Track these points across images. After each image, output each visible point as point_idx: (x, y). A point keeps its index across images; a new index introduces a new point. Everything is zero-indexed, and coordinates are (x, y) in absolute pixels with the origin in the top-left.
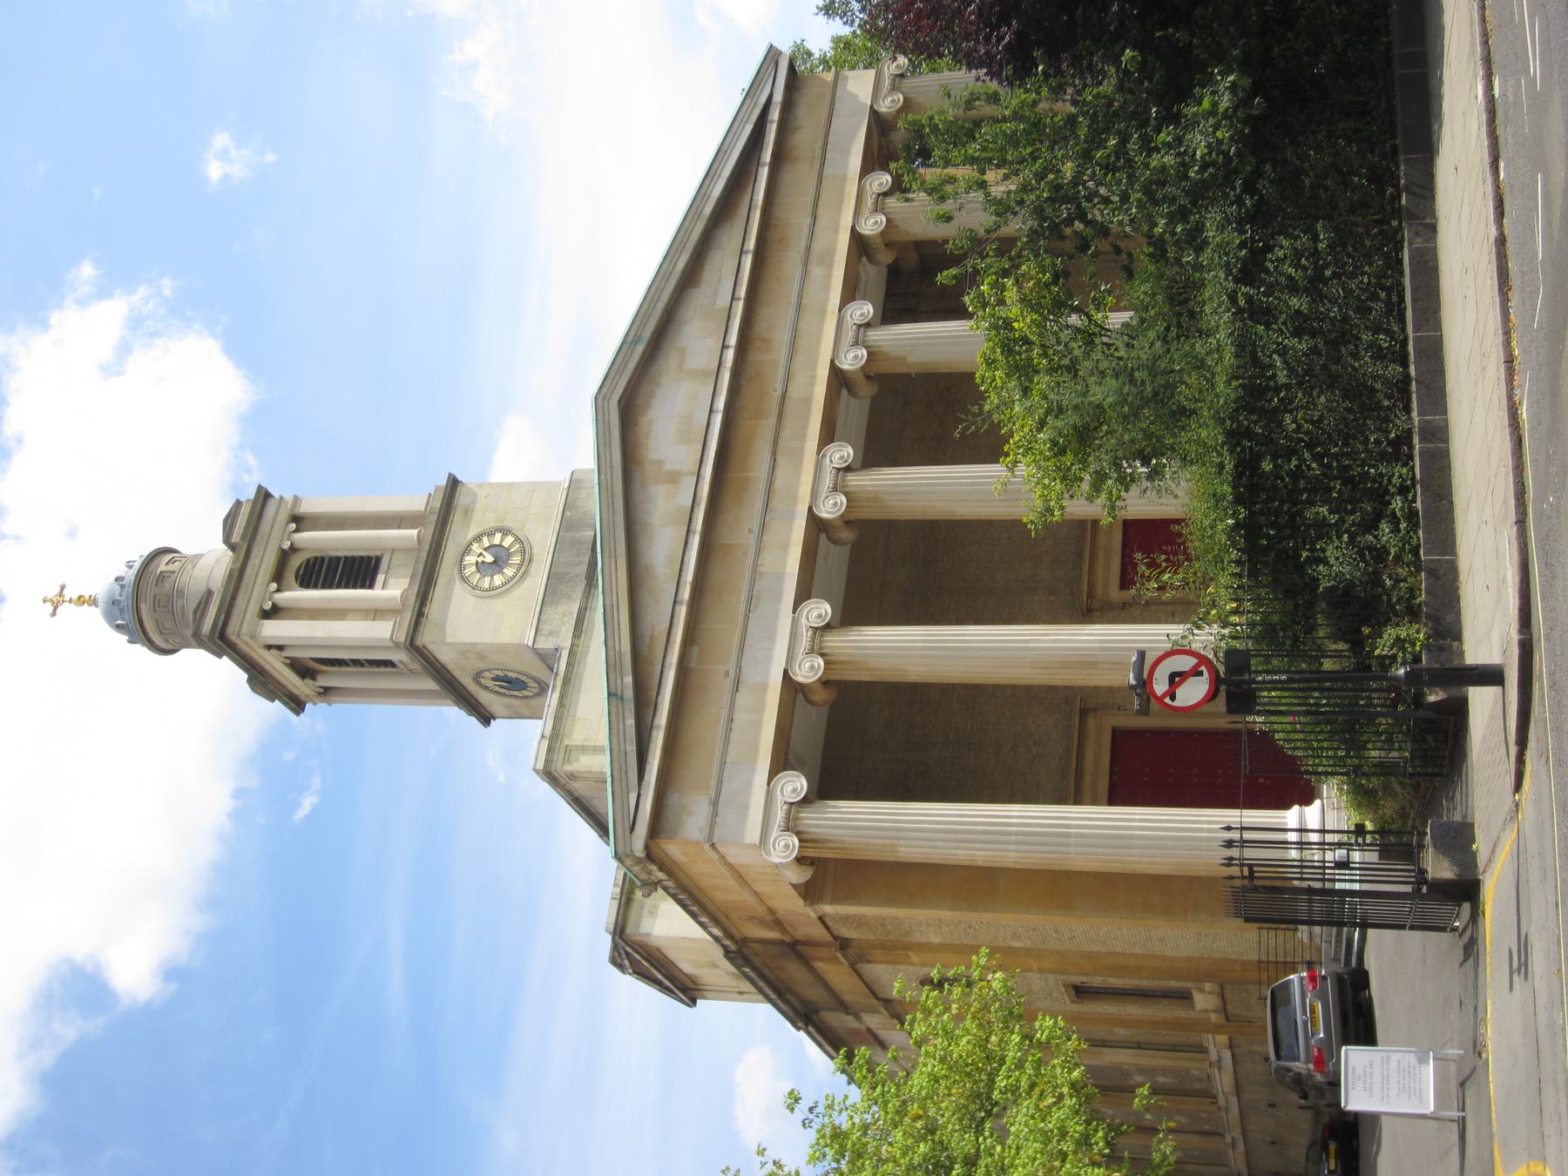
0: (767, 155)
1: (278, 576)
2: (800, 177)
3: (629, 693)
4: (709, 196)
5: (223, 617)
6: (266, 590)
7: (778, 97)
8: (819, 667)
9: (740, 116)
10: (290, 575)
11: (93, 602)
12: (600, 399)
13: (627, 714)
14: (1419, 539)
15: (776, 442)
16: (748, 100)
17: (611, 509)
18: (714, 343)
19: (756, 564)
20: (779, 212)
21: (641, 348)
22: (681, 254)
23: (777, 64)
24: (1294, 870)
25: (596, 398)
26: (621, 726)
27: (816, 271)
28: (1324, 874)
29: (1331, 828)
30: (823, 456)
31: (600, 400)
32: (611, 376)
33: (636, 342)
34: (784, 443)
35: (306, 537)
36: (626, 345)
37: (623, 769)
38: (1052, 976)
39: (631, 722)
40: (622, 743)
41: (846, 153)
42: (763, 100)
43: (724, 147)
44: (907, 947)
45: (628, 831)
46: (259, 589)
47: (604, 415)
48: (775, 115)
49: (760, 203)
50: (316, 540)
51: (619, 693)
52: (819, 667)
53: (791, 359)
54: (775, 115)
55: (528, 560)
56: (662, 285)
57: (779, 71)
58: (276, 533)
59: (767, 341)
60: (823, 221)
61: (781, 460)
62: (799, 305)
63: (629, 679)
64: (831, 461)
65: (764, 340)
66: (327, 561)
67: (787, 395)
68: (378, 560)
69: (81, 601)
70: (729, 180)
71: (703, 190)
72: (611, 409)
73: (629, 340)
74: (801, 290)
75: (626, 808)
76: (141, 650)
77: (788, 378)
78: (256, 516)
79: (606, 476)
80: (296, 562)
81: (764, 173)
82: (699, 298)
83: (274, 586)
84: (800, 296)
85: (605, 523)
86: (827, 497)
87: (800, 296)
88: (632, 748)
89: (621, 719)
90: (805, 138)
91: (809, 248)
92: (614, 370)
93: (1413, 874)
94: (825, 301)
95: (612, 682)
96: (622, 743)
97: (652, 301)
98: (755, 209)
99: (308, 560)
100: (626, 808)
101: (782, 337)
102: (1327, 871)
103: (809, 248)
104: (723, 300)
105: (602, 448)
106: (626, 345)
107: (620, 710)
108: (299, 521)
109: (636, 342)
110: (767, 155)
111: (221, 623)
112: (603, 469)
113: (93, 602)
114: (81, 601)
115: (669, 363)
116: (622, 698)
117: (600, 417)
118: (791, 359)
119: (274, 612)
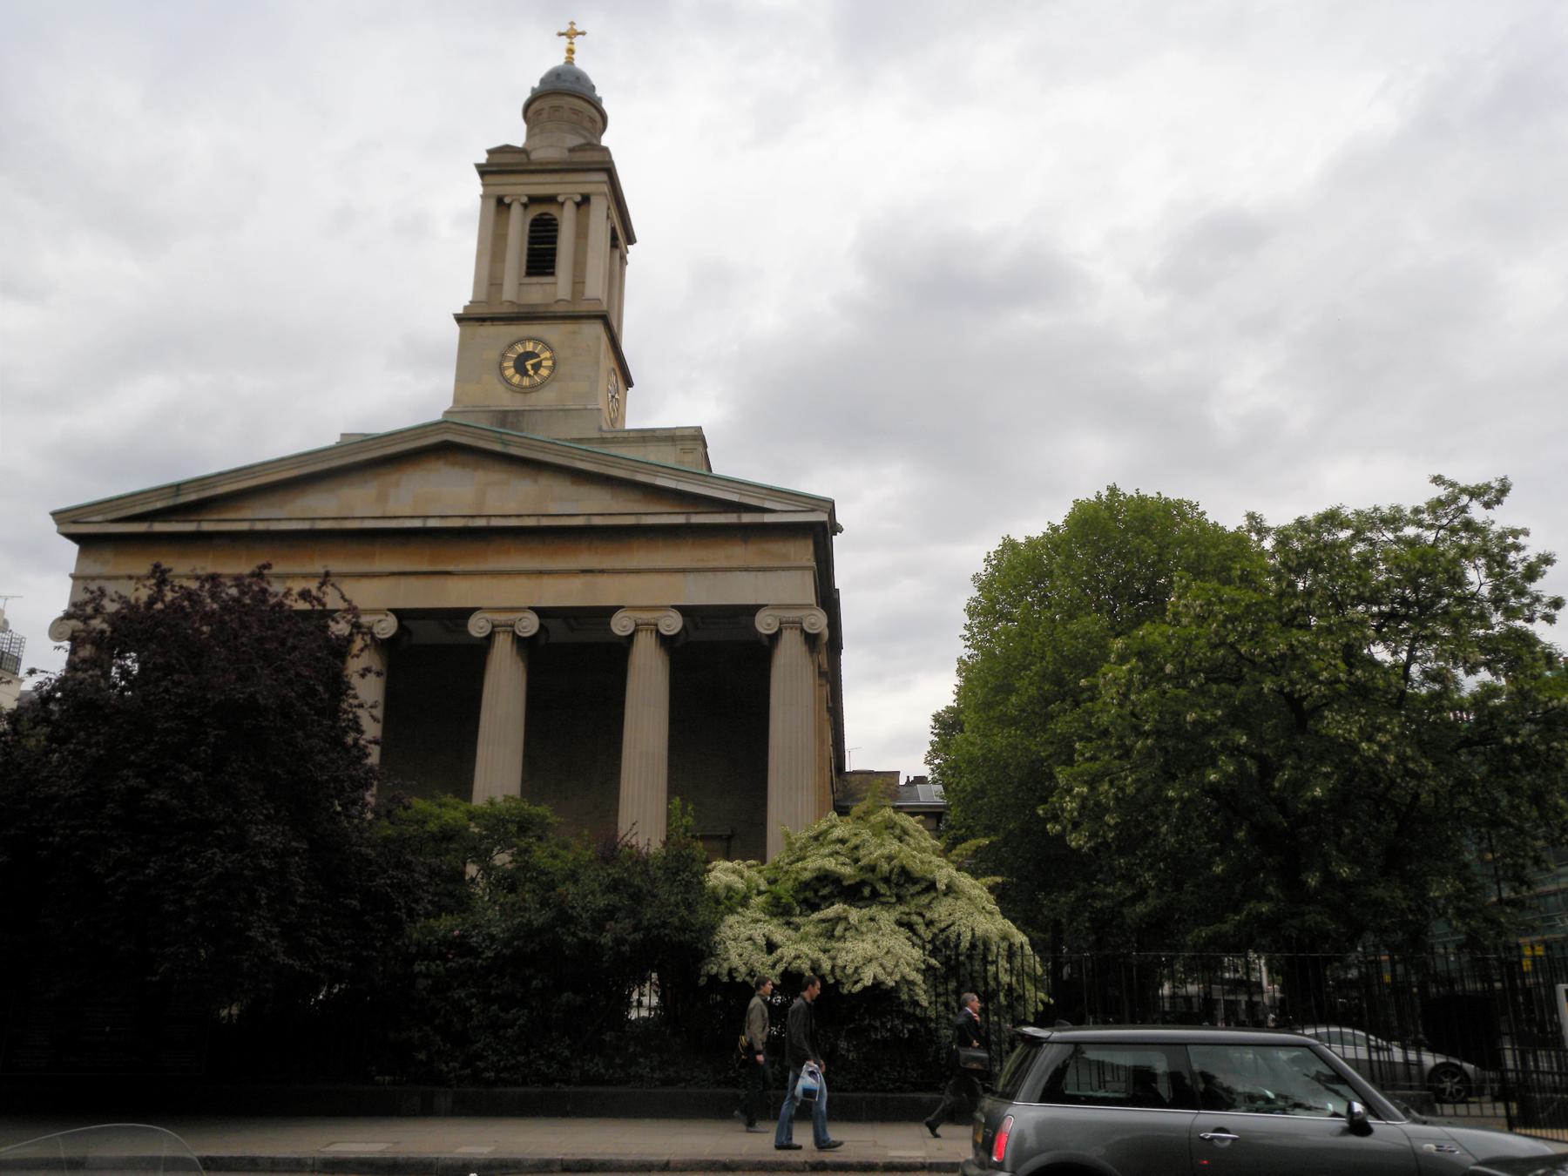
1: (534, 200)
3: (182, 500)
6: (520, 195)
7: (768, 518)
10: (536, 211)
11: (570, 61)
14: (891, 1091)
16: (764, 491)
23: (813, 510)
30: (387, 615)
39: (159, 505)
42: (767, 505)
44: (1320, 707)
45: (73, 519)
48: (747, 518)
50: (567, 220)
55: (525, 391)
57: (803, 514)
58: (570, 189)
63: (193, 497)
64: (380, 621)
66: (553, 234)
67: (449, 577)
69: (571, 51)
76: (527, 95)
78: (585, 167)
80: (552, 210)
83: (525, 200)
88: (138, 510)
90: (739, 553)
91: (602, 571)
93: (1553, 1053)
99: (555, 219)
103: (602, 571)
105: (399, 436)
113: (570, 61)
114: (571, 51)
117: (429, 429)
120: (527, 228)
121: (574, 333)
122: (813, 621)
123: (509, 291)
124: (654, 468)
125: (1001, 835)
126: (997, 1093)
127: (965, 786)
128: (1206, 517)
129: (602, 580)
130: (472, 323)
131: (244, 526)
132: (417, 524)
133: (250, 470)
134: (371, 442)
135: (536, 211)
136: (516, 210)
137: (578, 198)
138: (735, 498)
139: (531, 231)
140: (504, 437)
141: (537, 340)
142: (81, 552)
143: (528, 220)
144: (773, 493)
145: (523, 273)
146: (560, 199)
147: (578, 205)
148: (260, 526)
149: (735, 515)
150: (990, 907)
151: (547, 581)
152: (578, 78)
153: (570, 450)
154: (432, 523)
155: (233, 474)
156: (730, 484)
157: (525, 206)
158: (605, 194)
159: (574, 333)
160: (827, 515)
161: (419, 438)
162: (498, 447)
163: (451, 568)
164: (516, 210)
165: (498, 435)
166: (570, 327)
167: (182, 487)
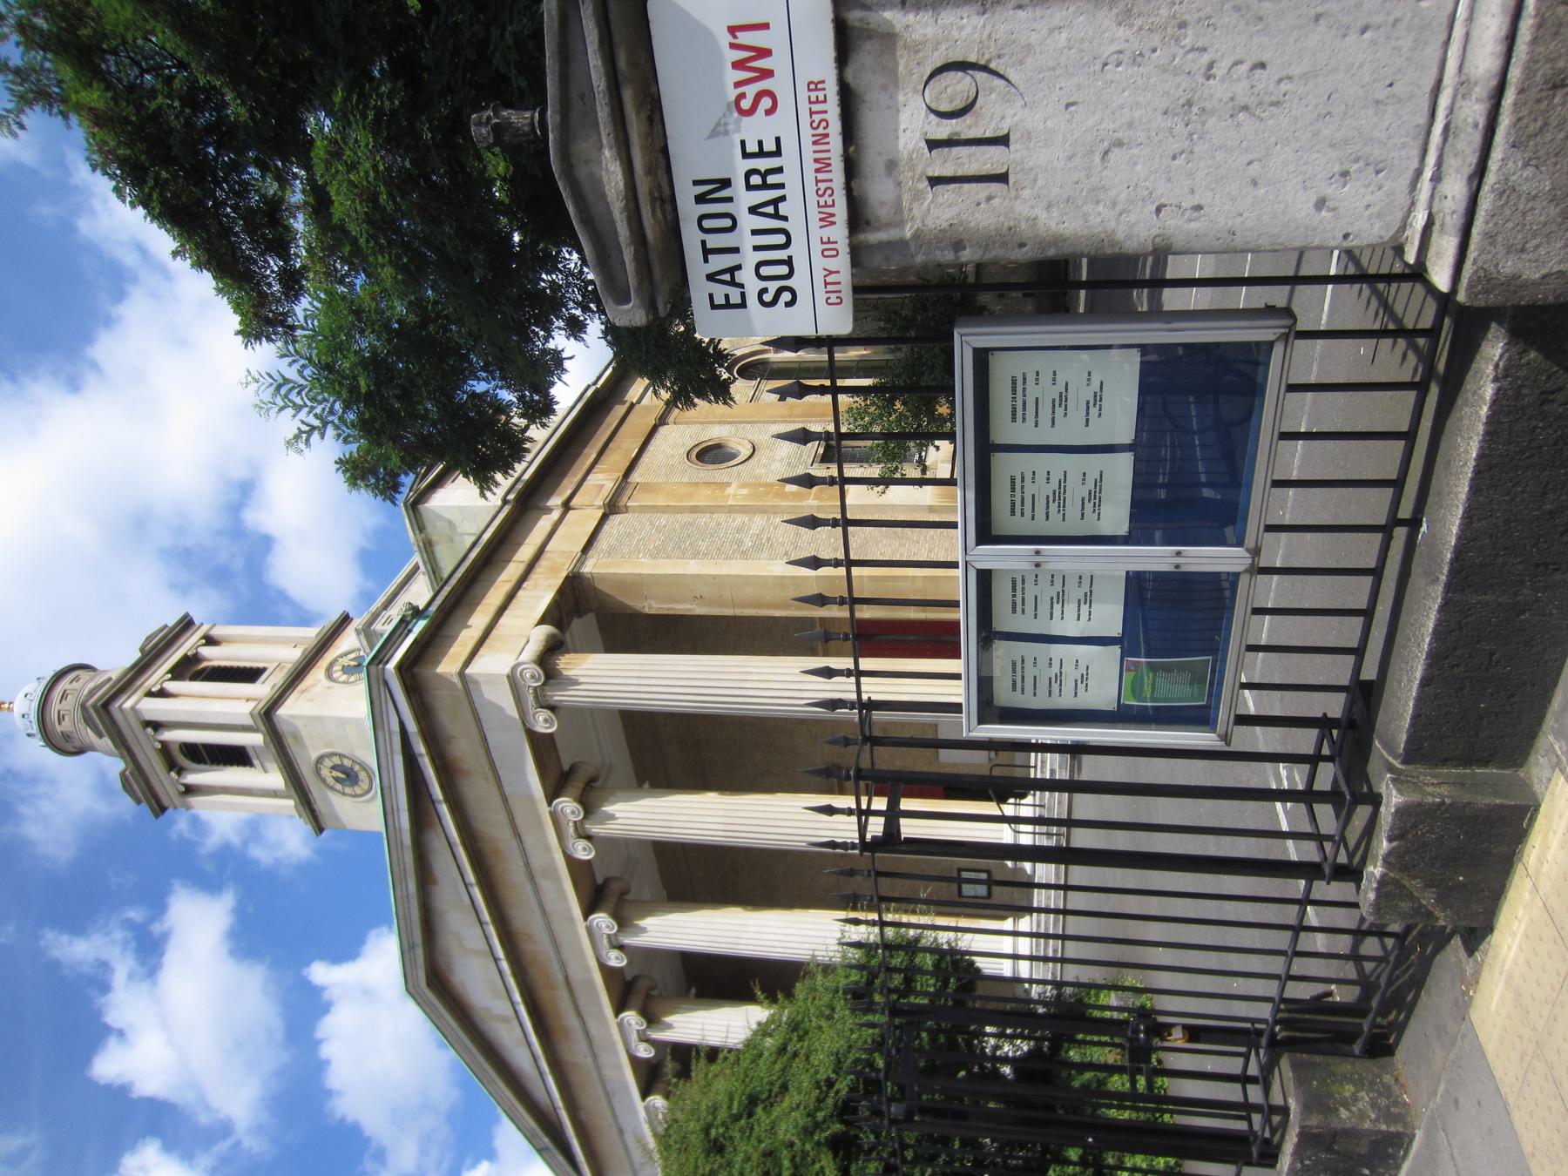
0: (437, 791)
2: (477, 791)
4: (400, 829)
5: (153, 802)
7: (412, 727)
8: (539, 674)
9: (382, 751)
12: (411, 989)
15: (577, 1008)
16: (380, 734)
19: (601, 1077)
21: (420, 951)
22: (406, 878)
23: (386, 684)
25: (407, 990)
27: (546, 885)
31: (411, 989)
32: (409, 972)
33: (412, 947)
34: (584, 1008)
35: (206, 651)
36: (406, 954)
38: (893, 929)
39: (561, 1158)
41: (522, 771)
42: (396, 727)
46: (158, 676)
47: (421, 997)
48: (420, 748)
50: (215, 656)
52: (539, 674)
54: (420, 748)
56: (406, 906)
60: (528, 839)
61: (588, 1019)
62: (544, 913)
65: (526, 935)
68: (264, 670)
70: (410, 810)
73: (406, 948)
77: (563, 966)
81: (444, 809)
85: (472, 1066)
90: (463, 748)
91: (527, 865)
92: (408, 965)
94: (569, 910)
97: (405, 920)
98: (456, 846)
105: (436, 1021)
106: (406, 954)
108: (210, 641)
110: (437, 791)
112: (446, 1033)
117: (420, 1000)
119: (162, 694)
128: (238, 328)
133: (509, 1111)
135: (182, 760)
137: (150, 730)
138: (399, 761)
141: (317, 771)
144: (378, 726)
150: (1062, 226)
152: (442, 610)
155: (516, 1121)
156: (384, 764)
157: (181, 771)
158: (906, 46)
159: (329, 688)
160: (973, 281)
161: (434, 1006)
163: (560, 977)
164: (192, 778)
167: (539, 1147)
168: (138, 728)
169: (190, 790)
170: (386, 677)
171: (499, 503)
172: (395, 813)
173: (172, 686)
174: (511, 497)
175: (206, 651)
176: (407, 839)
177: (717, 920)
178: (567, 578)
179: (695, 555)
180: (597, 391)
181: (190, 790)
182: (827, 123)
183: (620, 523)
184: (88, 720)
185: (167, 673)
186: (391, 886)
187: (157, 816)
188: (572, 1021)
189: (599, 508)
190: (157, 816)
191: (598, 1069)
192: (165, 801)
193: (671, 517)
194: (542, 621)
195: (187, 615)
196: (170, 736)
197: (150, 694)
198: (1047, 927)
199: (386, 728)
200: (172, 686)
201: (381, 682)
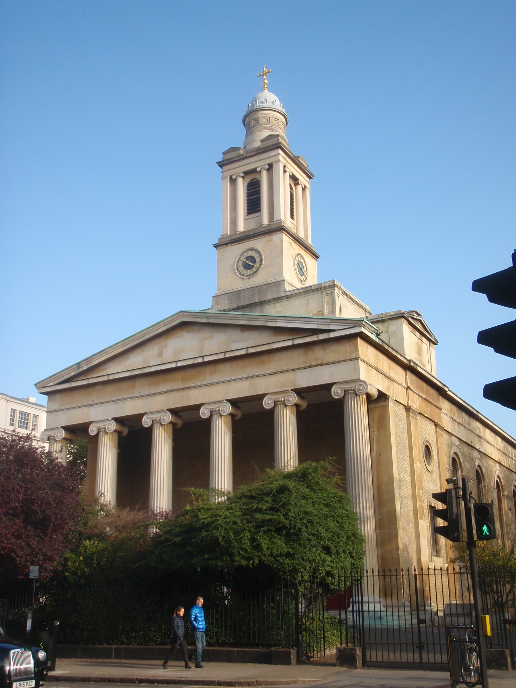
1: (246, 173)
7: (332, 335)
13: (75, 372)
16: (329, 321)
17: (140, 337)
18: (215, 350)
20: (278, 355)
23: (354, 327)
24: (360, 597)
25: (181, 312)
26: (71, 371)
28: (356, 612)
29: (370, 614)
37: (59, 377)
40: (65, 374)
42: (332, 328)
43: (301, 319)
45: (42, 386)
47: (176, 318)
48: (322, 337)
49: (272, 347)
51: (80, 367)
53: (206, 385)
54: (322, 337)
59: (214, 373)
65: (215, 371)
71: (278, 318)
72: (180, 319)
74: (237, 380)
75: (48, 383)
79: (152, 329)
81: (289, 343)
82: (236, 334)
84: (234, 380)
86: (207, 409)
87: (234, 380)
88: (65, 377)
89: (73, 370)
90: (319, 354)
91: (257, 376)
95: (82, 363)
96: (65, 374)
99: (259, 181)
100: (48, 383)
101: (215, 378)
102: (358, 613)
103: (257, 376)
104: (234, 347)
107: (75, 369)
109: (207, 317)
111: (235, 159)
112: (154, 327)
115: (206, 333)
116: (79, 368)
117: (174, 317)
118: (206, 385)
119: (285, 171)
120: (246, 188)
121: (270, 241)
122: (361, 388)
123: (241, 227)
124: (275, 318)
125: (225, 545)
126: (493, 632)
127: (56, 557)
129: (259, 380)
130: (222, 247)
131: (105, 379)
132: (173, 365)
134: (151, 328)
135: (249, 179)
136: (240, 181)
137: (267, 167)
139: (248, 190)
140: (206, 315)
142: (49, 399)
143: (246, 185)
145: (246, 214)
146: (258, 170)
147: (268, 170)
148: (111, 377)
149: (315, 336)
151: (233, 385)
153: (236, 316)
154: (180, 364)
157: (243, 177)
162: (205, 320)
163: (191, 385)
164: (240, 181)
165: (204, 314)
166: (267, 238)
168: (269, 161)
169: (233, 181)
170: (357, 327)
171: (409, 359)
172: (286, 321)
173: (287, 175)
174: (412, 364)
175: (300, 188)
176: (269, 324)
177: (166, 449)
178: (386, 395)
179: (397, 453)
180: (445, 391)
181: (233, 181)
182: (306, 279)
183: (403, 414)
184: (271, 137)
185: (292, 173)
186: (244, 314)
187: (218, 163)
188: (162, 388)
189: (408, 404)
190: (218, 163)
191: (132, 398)
192: (226, 168)
193: (407, 438)
194: (379, 391)
195: (314, 176)
196: (264, 174)
197: (285, 167)
198: (455, 601)
199: (331, 324)
200: (287, 175)
201: (356, 325)
